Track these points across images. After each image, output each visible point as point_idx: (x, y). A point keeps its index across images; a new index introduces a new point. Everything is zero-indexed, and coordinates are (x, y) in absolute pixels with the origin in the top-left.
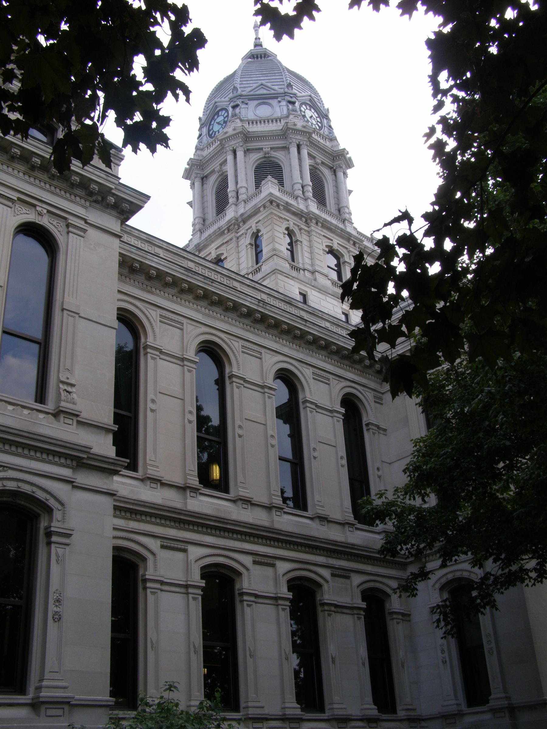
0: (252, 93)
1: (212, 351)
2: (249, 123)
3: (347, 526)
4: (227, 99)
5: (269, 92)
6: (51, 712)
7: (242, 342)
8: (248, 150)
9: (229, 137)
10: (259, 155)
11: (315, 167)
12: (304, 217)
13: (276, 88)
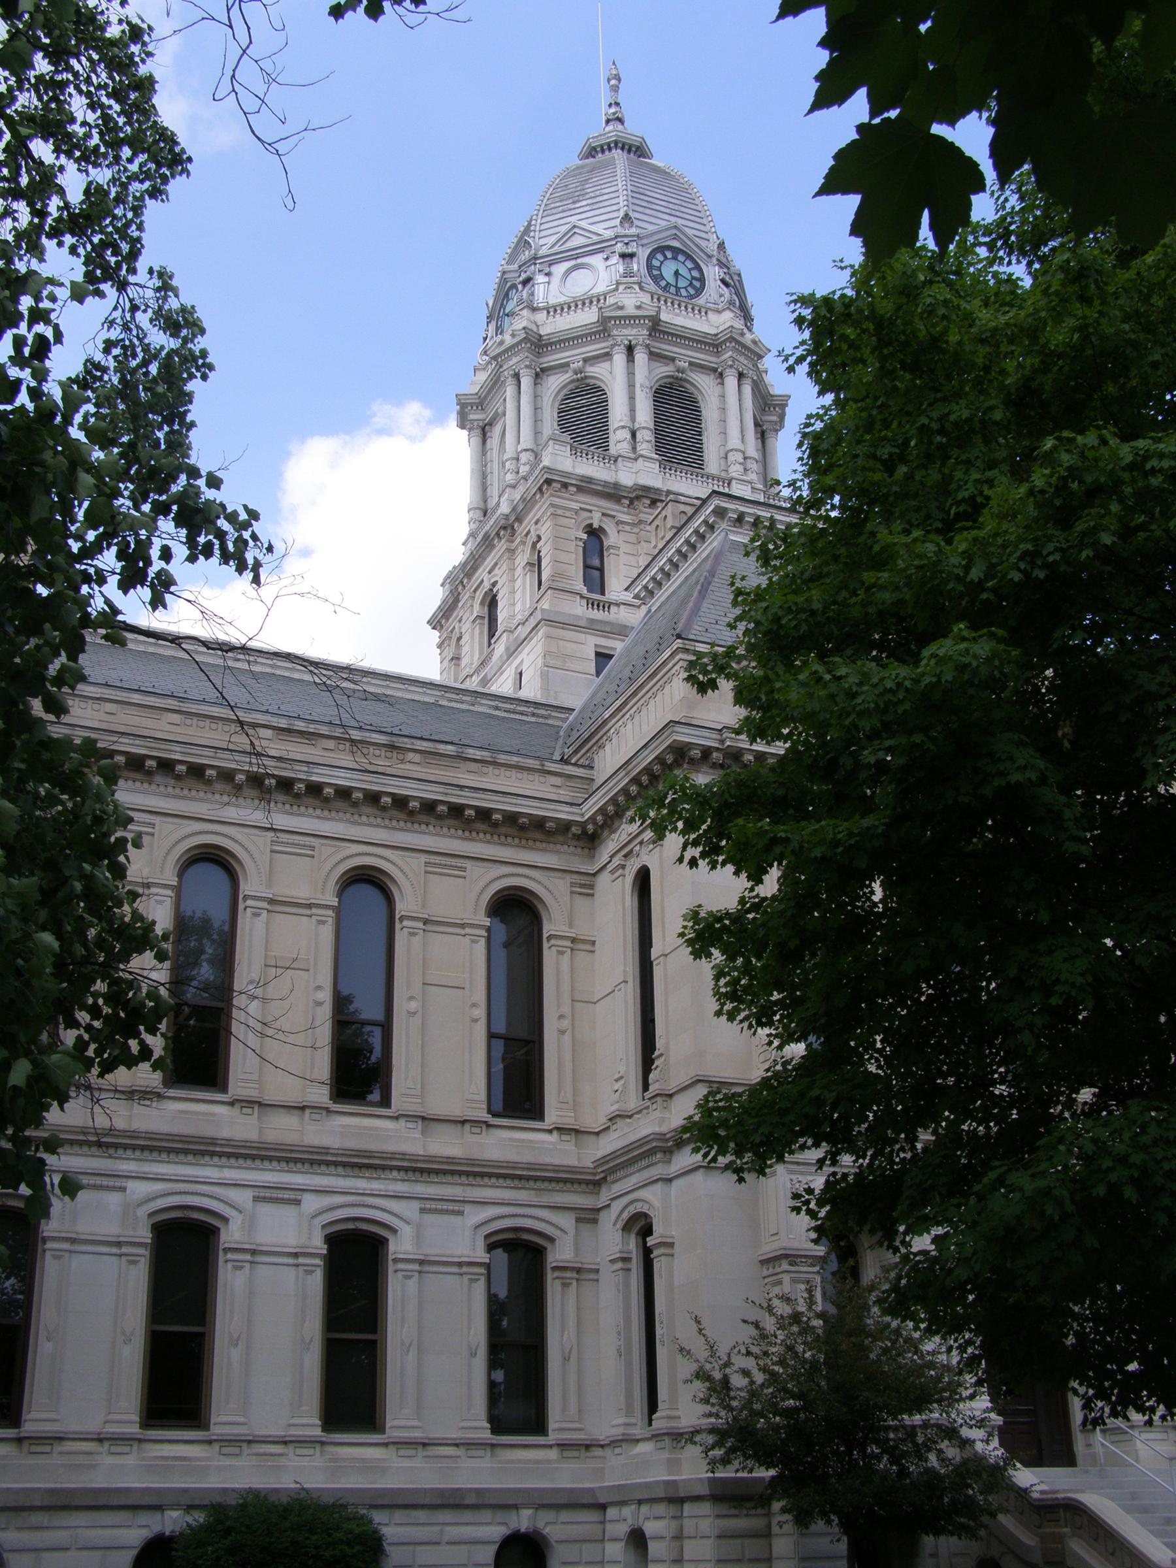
0: (556, 249)
3: (467, 1126)
4: (516, 266)
5: (589, 241)
6: (34, 1449)
7: (423, 858)
8: (543, 370)
12: (625, 497)
13: (598, 228)
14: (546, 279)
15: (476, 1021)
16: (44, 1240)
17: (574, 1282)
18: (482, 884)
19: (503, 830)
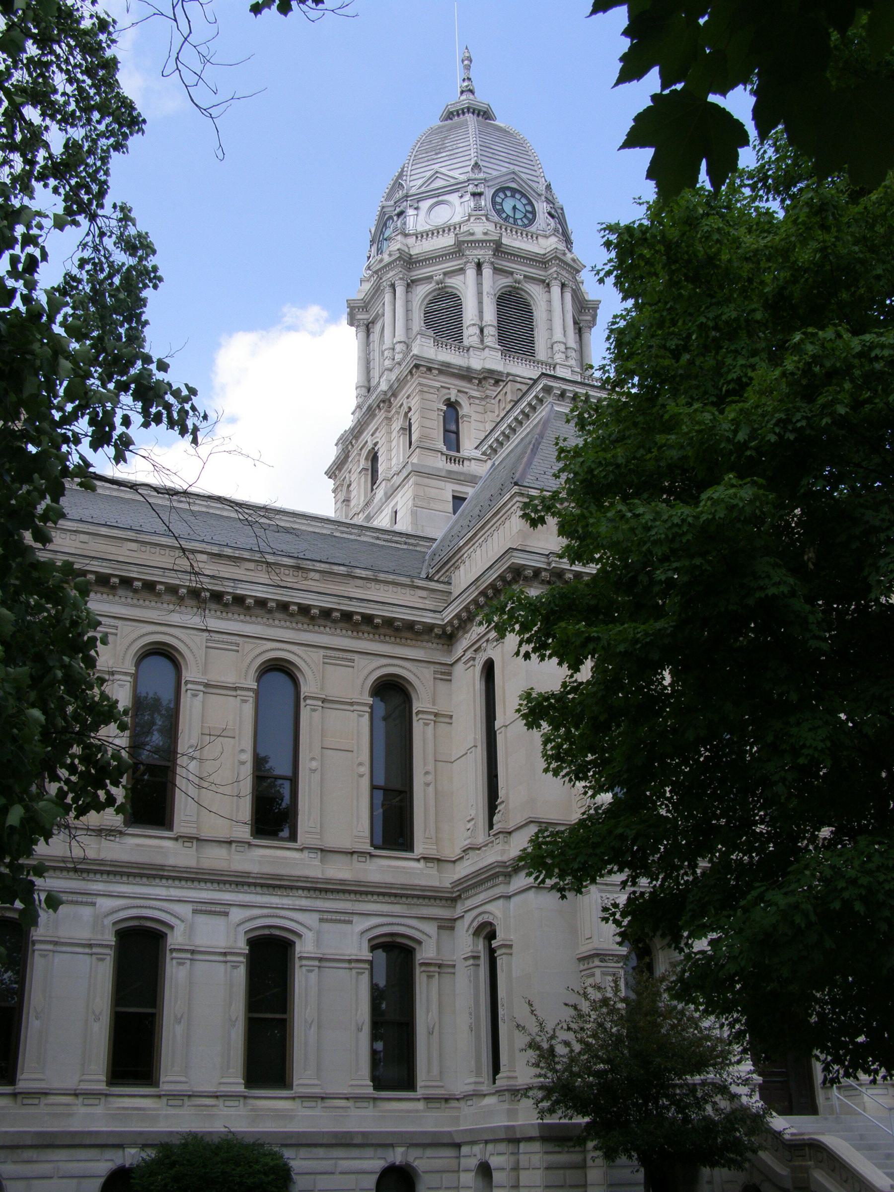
0: (423, 189)
1: (279, 669)
2: (417, 237)
4: (392, 203)
5: (448, 183)
7: (322, 652)
9: (475, 241)
10: (431, 286)
11: (515, 288)
12: (475, 378)
13: (455, 174)
14: (415, 212)
15: (361, 776)
16: (34, 943)
17: (437, 975)
18: (366, 672)
19: (382, 631)
